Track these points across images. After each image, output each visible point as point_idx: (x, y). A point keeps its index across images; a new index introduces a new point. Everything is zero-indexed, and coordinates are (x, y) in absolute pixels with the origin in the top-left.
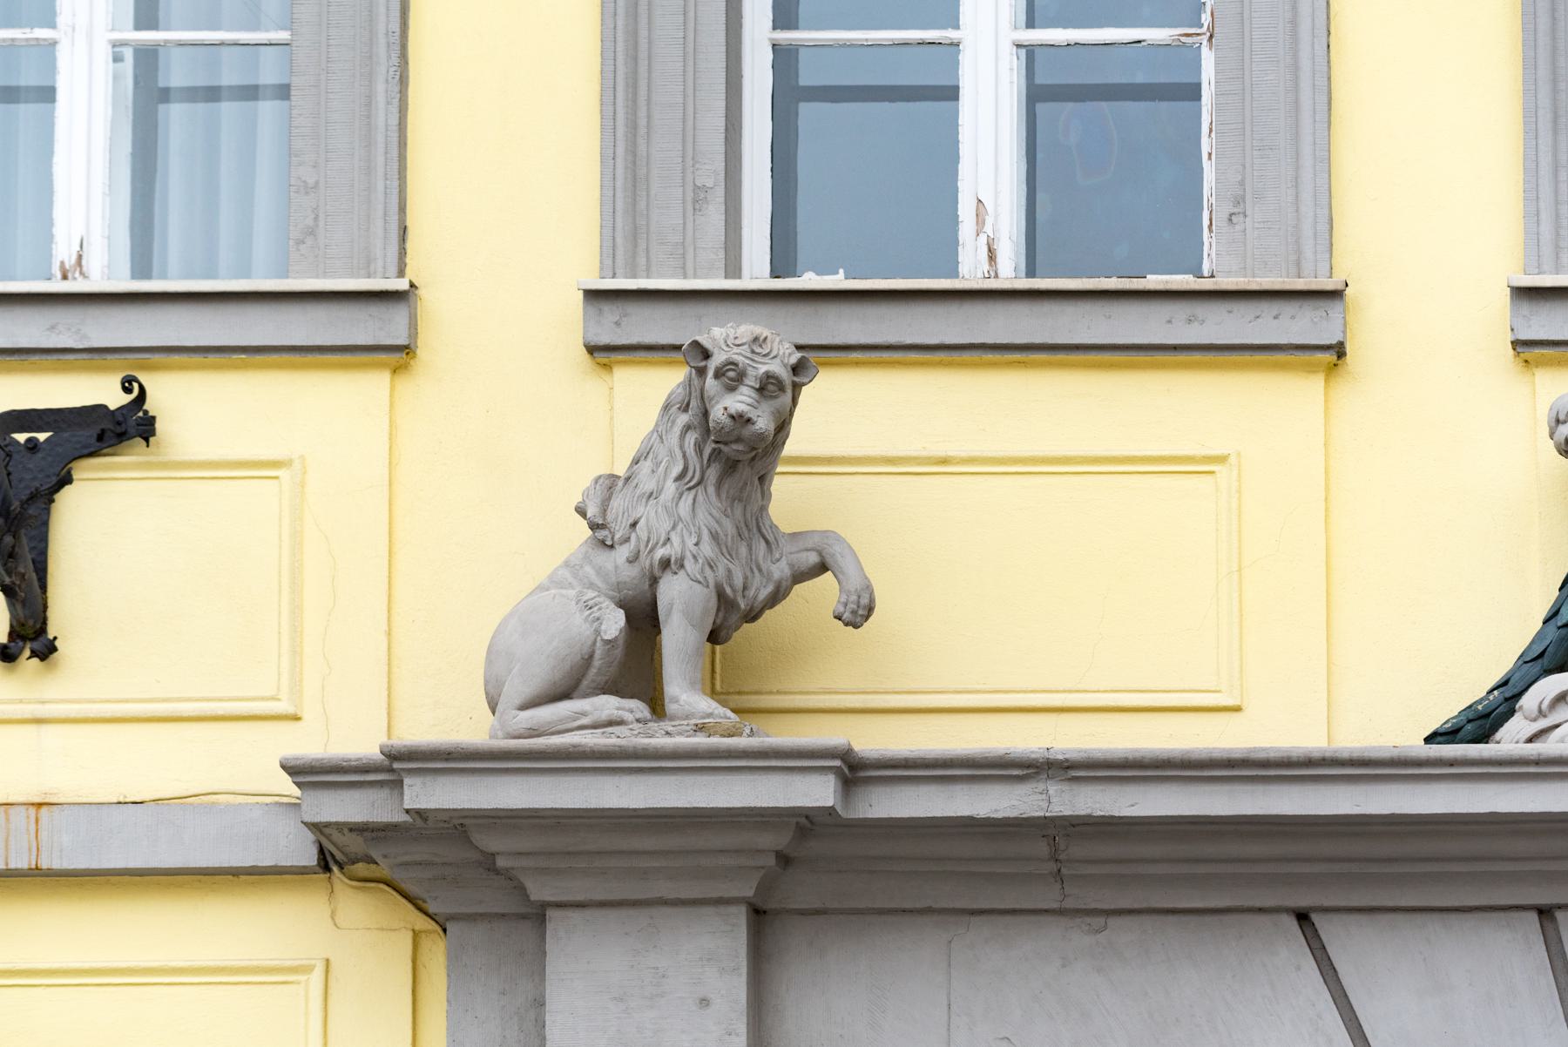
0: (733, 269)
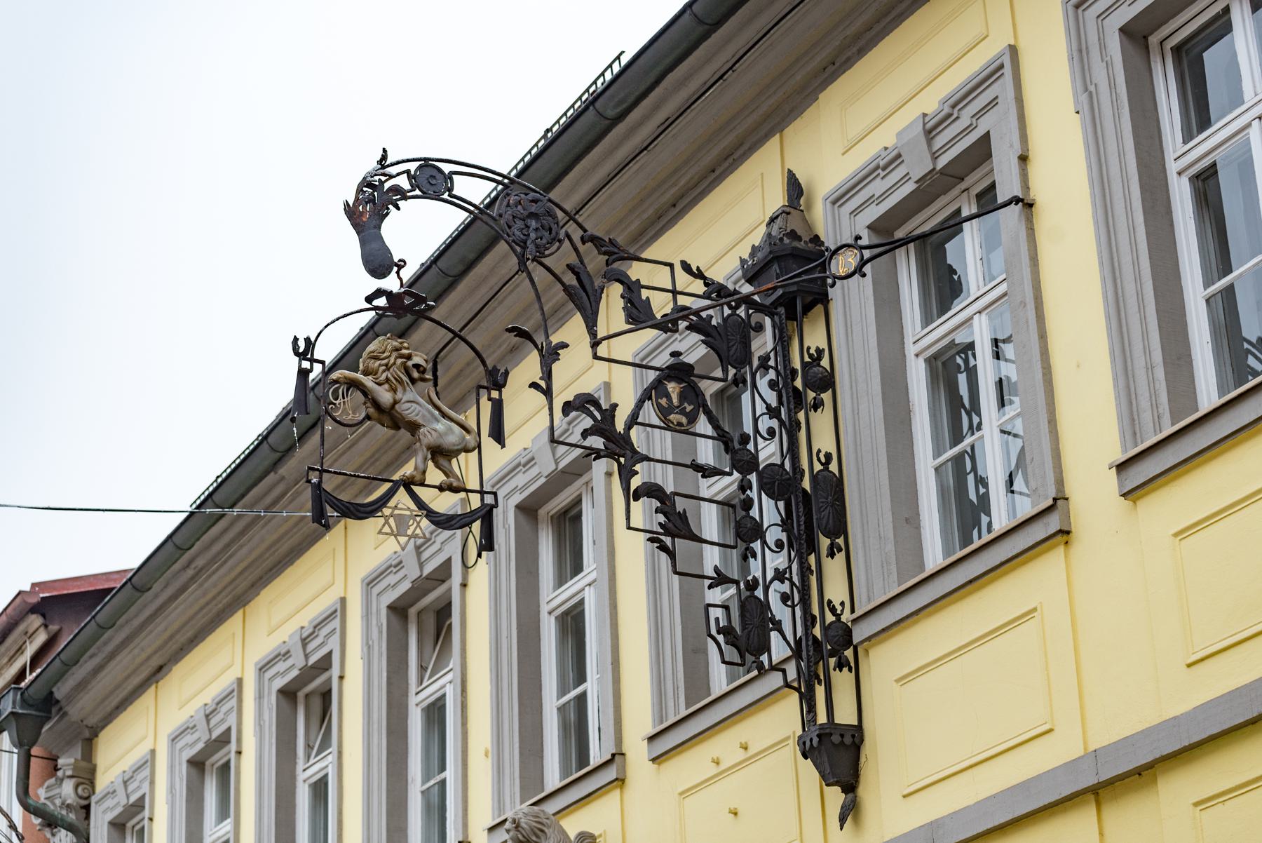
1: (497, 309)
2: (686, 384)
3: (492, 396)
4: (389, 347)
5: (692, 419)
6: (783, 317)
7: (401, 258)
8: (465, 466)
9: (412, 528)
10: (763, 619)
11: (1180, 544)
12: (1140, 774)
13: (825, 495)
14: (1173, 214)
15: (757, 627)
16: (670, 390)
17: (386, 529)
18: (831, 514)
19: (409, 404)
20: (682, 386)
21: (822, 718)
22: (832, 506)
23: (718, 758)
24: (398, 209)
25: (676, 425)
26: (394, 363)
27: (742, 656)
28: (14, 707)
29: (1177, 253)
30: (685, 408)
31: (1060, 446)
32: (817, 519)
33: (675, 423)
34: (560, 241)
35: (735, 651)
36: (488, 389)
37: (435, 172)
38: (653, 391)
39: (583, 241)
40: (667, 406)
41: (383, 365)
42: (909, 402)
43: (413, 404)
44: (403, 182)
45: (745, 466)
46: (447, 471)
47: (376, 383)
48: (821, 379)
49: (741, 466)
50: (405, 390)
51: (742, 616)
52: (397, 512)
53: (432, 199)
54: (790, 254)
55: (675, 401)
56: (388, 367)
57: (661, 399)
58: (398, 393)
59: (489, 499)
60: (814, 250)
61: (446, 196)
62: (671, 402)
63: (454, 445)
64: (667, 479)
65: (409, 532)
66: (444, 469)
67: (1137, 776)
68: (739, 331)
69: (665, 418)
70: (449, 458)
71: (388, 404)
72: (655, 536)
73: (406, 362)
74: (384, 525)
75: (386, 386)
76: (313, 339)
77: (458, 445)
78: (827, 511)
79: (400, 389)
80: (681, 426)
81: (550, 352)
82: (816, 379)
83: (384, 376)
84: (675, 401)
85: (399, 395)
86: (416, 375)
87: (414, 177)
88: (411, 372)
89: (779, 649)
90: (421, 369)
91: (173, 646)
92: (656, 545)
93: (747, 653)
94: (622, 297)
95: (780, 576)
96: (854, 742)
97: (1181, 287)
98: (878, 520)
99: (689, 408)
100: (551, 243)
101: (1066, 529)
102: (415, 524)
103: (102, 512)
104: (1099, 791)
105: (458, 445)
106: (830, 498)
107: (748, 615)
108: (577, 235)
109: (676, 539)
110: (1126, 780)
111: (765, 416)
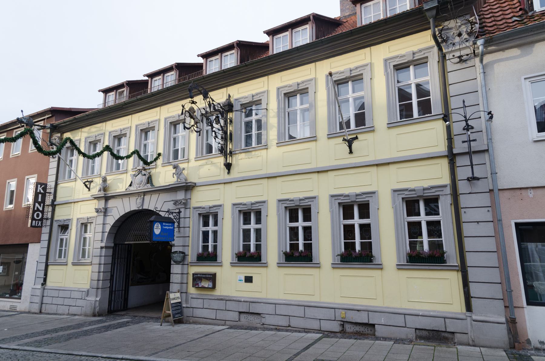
0: (285, 140)
21: (228, 162)
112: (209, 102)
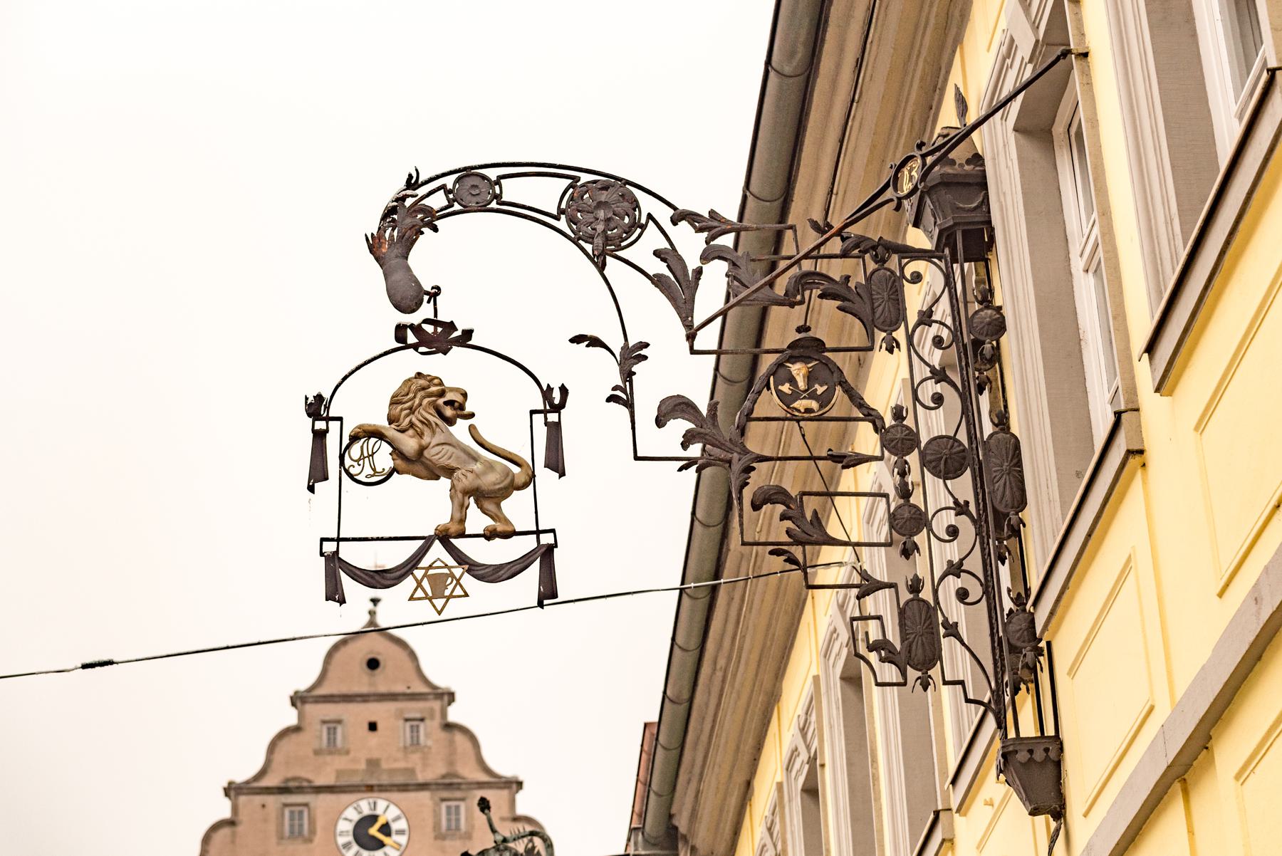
1: (820, 320)
2: (817, 362)
3: (550, 420)
4: (413, 388)
5: (824, 400)
6: (949, 259)
7: (434, 285)
8: (517, 508)
9: (450, 587)
10: (931, 624)
11: (1201, 439)
12: (1207, 748)
13: (998, 462)
14: (1197, 21)
15: (921, 636)
16: (794, 373)
17: (420, 593)
18: (1008, 483)
19: (440, 448)
20: (810, 365)
21: (1012, 734)
22: (1009, 474)
23: (991, 799)
24: (435, 229)
25: (804, 413)
26: (420, 405)
27: (904, 674)
28: (636, 850)
29: (1201, 69)
30: (816, 390)
31: (1131, 345)
32: (989, 493)
33: (803, 411)
34: (643, 227)
35: (893, 666)
36: (544, 412)
37: (476, 181)
38: (772, 378)
39: (675, 221)
40: (790, 392)
41: (406, 409)
42: (1078, 329)
43: (444, 447)
44: (438, 201)
45: (899, 445)
46: (493, 515)
47: (397, 430)
48: (989, 324)
49: (894, 447)
50: (434, 432)
51: (902, 625)
52: (431, 572)
53: (475, 211)
54: (940, 183)
55: (802, 384)
56: (412, 410)
57: (783, 385)
58: (425, 438)
59: (547, 539)
60: (974, 172)
61: (494, 205)
62: (797, 387)
63: (495, 484)
64: (791, 479)
65: (447, 593)
66: (490, 513)
67: (1205, 750)
68: (887, 287)
69: (788, 407)
70: (496, 500)
71: (413, 451)
72: (776, 547)
73: (436, 400)
74: (416, 590)
75: (411, 432)
76: (327, 395)
77: (499, 484)
78: (1002, 481)
79: (427, 432)
80: (811, 413)
81: (626, 356)
82: (983, 324)
83: (407, 420)
84: (802, 384)
85: (426, 440)
86: (449, 412)
87: (450, 192)
88: (442, 410)
89: (955, 660)
90: (456, 404)
91: (745, 758)
92: (783, 558)
93: (908, 666)
94: (727, 275)
95: (955, 569)
96: (1047, 756)
97: (1209, 111)
98: (1047, 480)
99: (820, 390)
100: (629, 232)
101: (1136, 447)
102: (455, 582)
103: (421, 626)
104: (1186, 776)
105: (499, 484)
106: (1006, 464)
107: (908, 623)
108: (664, 215)
109: (806, 547)
110: (1199, 757)
111: (929, 381)
112: (668, 255)
